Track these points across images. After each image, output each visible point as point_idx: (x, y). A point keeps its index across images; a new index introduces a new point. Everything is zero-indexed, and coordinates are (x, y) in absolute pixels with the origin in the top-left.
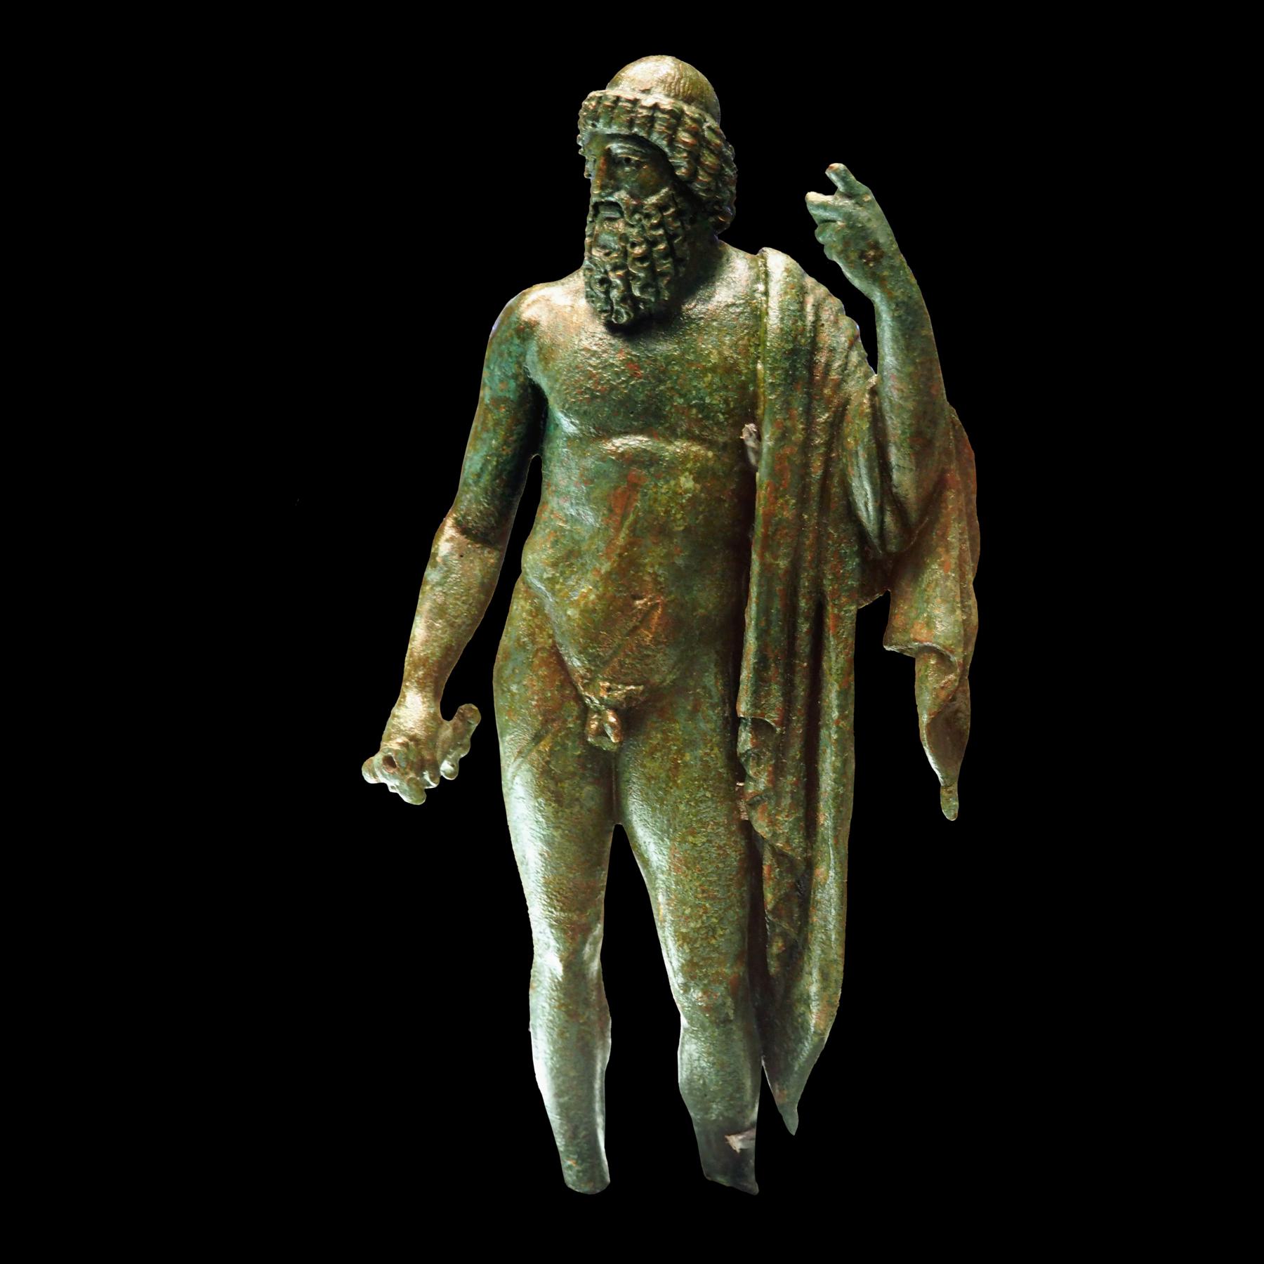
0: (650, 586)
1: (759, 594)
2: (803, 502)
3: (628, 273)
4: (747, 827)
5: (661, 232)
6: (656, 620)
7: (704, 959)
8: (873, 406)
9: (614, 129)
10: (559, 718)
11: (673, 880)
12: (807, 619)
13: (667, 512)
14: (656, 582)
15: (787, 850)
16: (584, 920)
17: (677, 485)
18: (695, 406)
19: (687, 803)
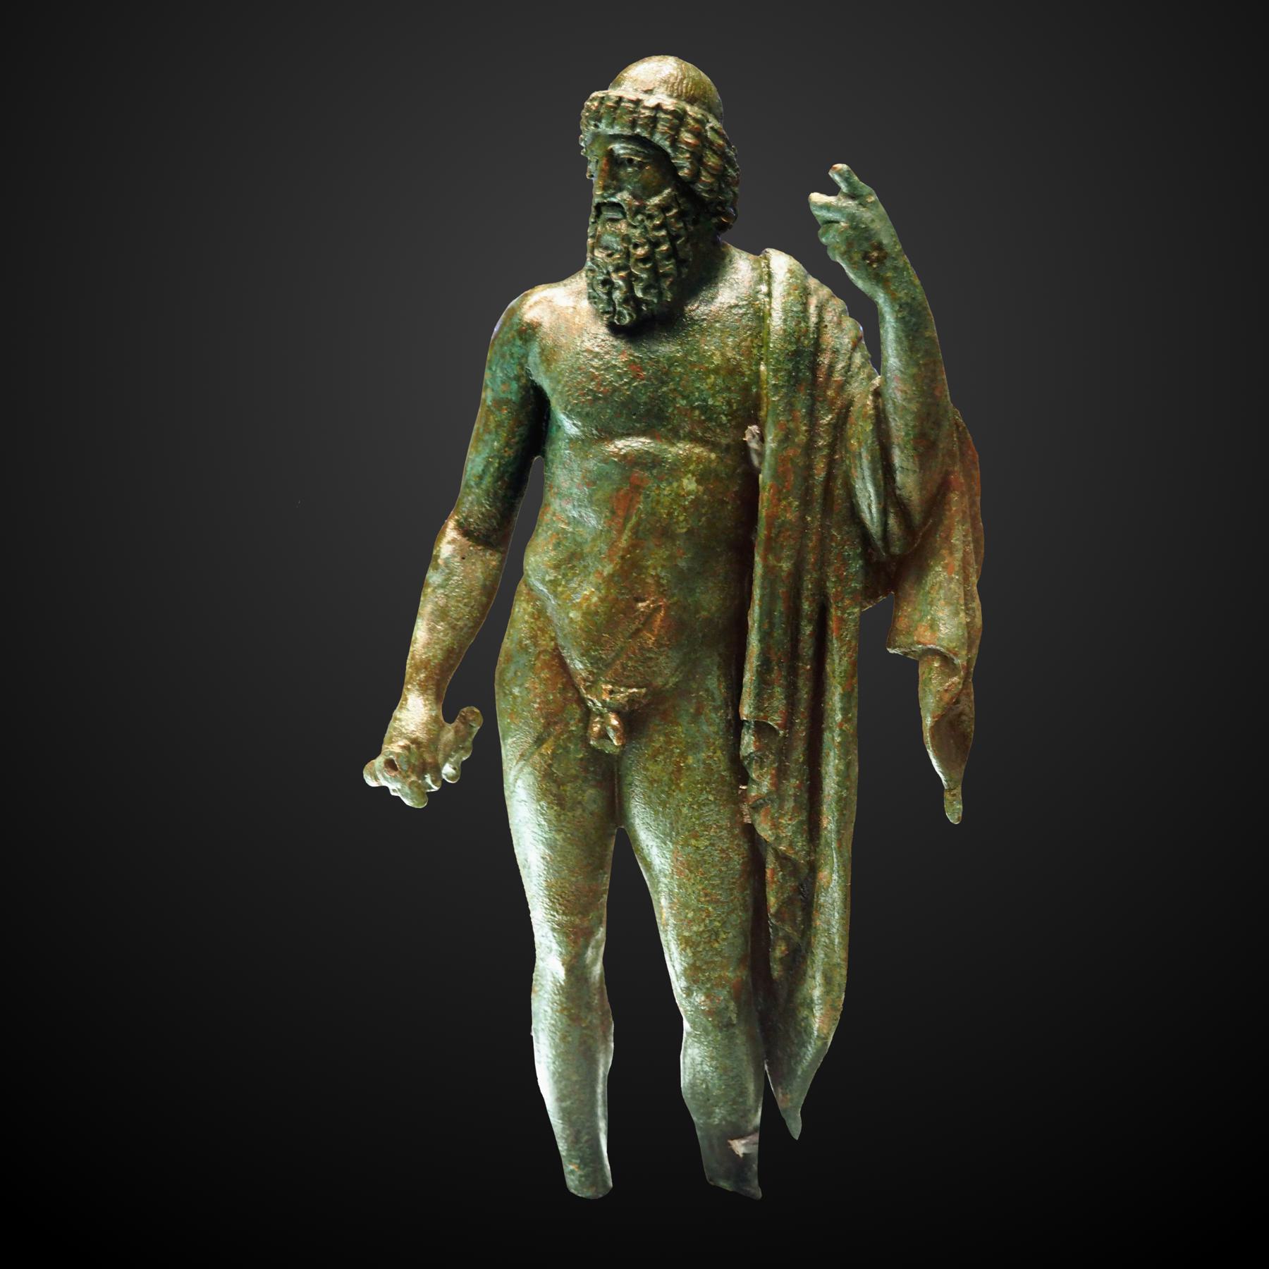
0: (653, 588)
1: (762, 596)
2: (806, 504)
3: (630, 274)
4: (750, 830)
5: (663, 233)
6: (658, 622)
7: (706, 963)
8: (876, 408)
9: (617, 130)
10: (561, 721)
11: (675, 884)
12: (810, 621)
13: (670, 514)
14: (659, 585)
15: (790, 854)
16: (586, 924)
17: (680, 486)
18: (698, 407)
19: (690, 807)
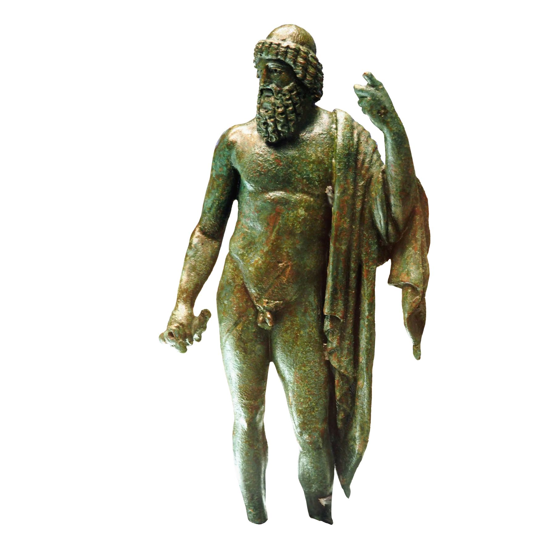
0: (286, 257)
1: (333, 261)
2: (352, 221)
3: (276, 120)
4: (328, 363)
5: (290, 102)
6: (288, 272)
7: (309, 421)
8: (383, 178)
9: (270, 57)
10: (245, 315)
11: (295, 386)
12: (354, 272)
13: (293, 225)
14: (288, 256)
15: (346, 373)
16: (256, 404)
17: (297, 213)
18: (305, 178)
19: (302, 353)
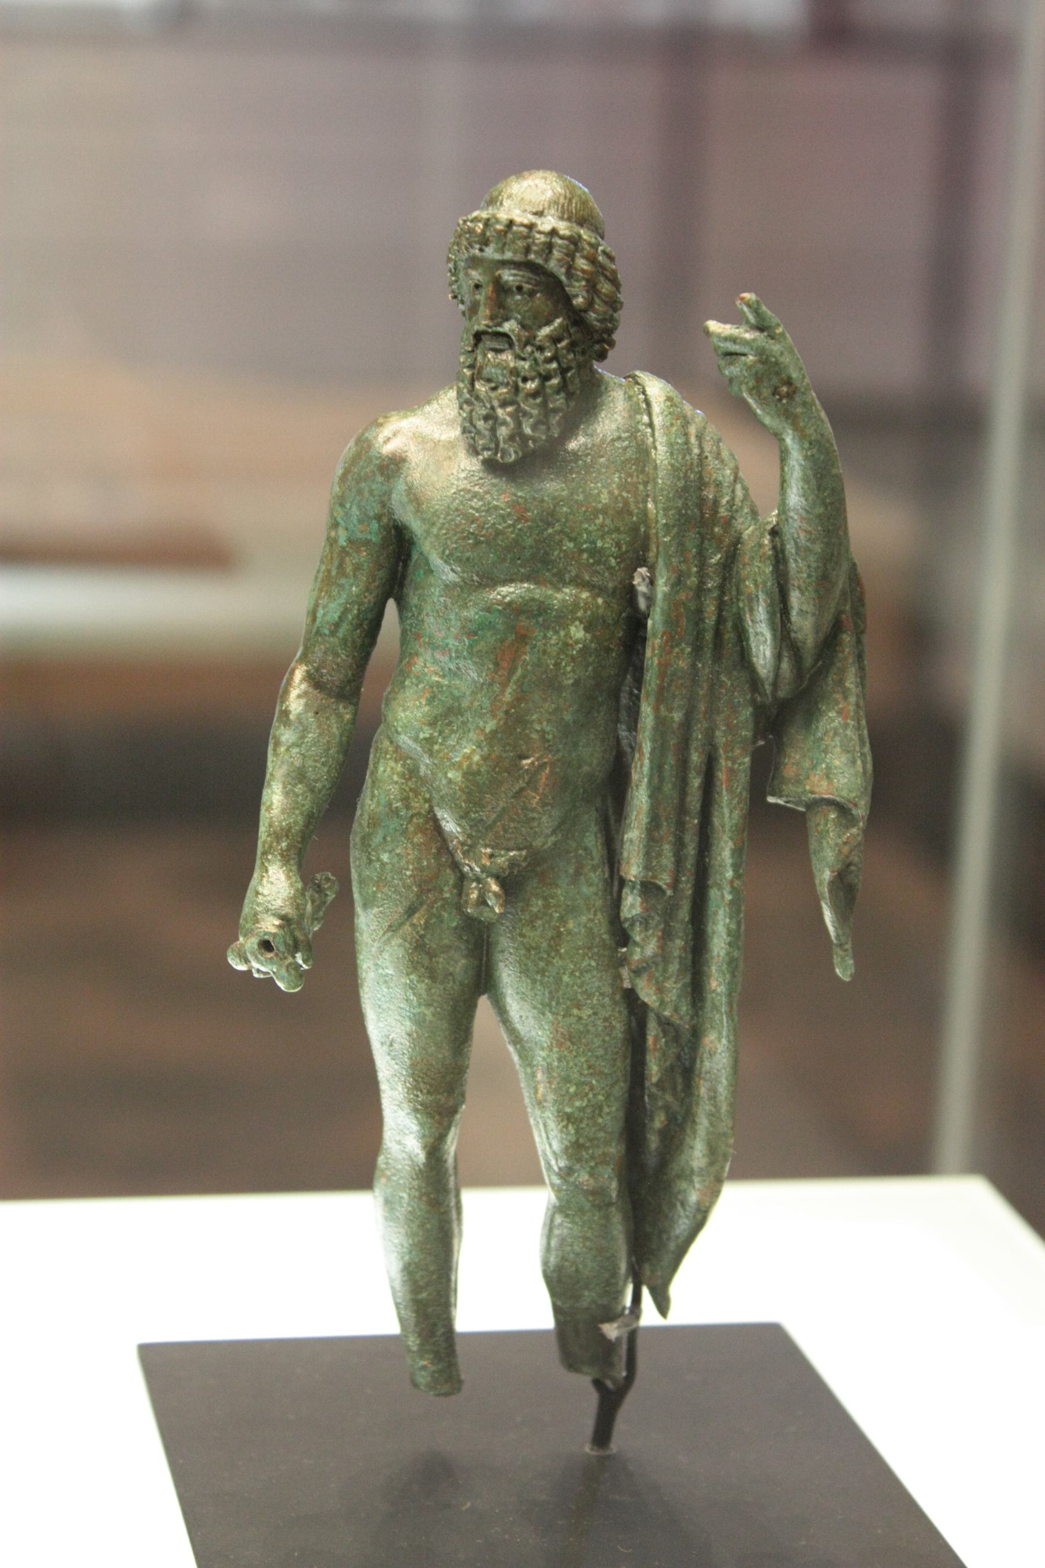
0: (538, 744)
2: (697, 649)
3: (519, 410)
4: (630, 997)
5: (554, 365)
7: (590, 1140)
8: (774, 548)
9: (508, 255)
10: (435, 889)
11: (555, 1056)
13: (557, 665)
15: (676, 1020)
16: (451, 1103)
17: (568, 635)
19: (572, 974)
